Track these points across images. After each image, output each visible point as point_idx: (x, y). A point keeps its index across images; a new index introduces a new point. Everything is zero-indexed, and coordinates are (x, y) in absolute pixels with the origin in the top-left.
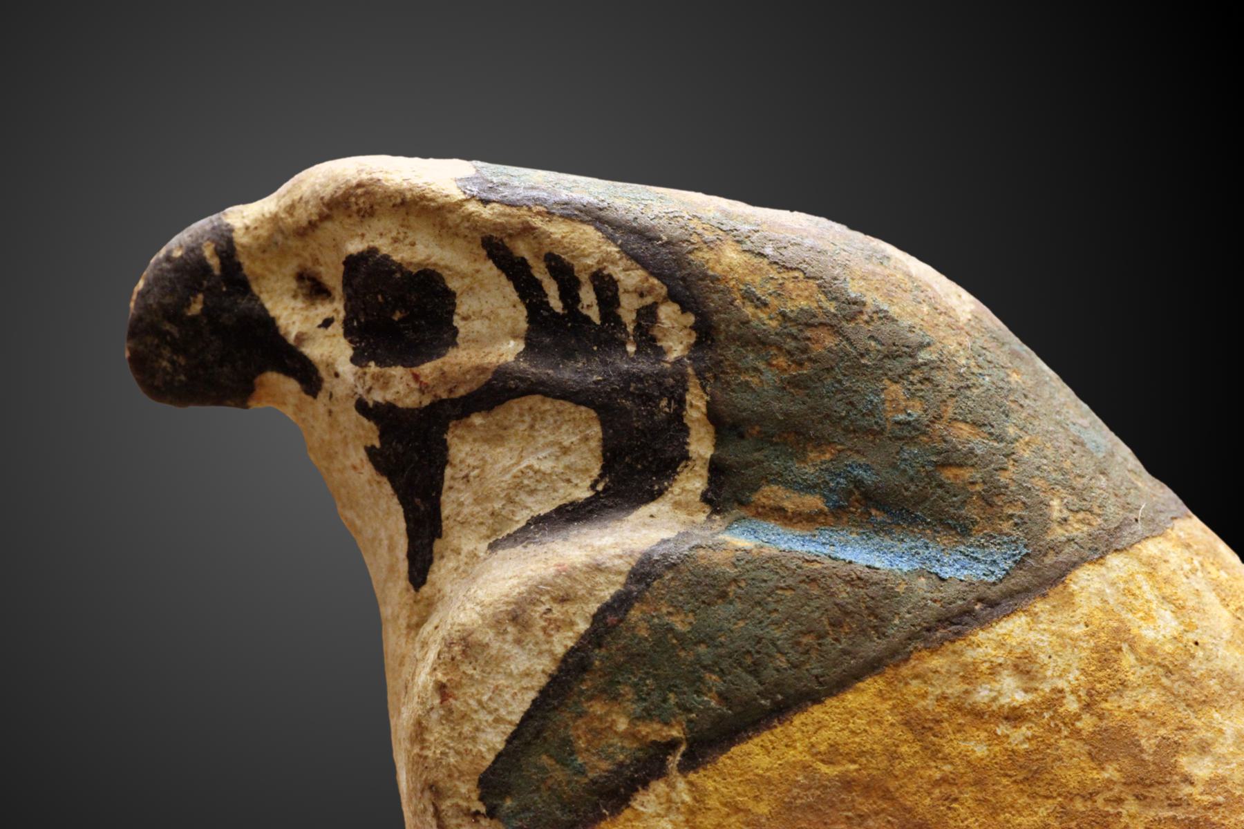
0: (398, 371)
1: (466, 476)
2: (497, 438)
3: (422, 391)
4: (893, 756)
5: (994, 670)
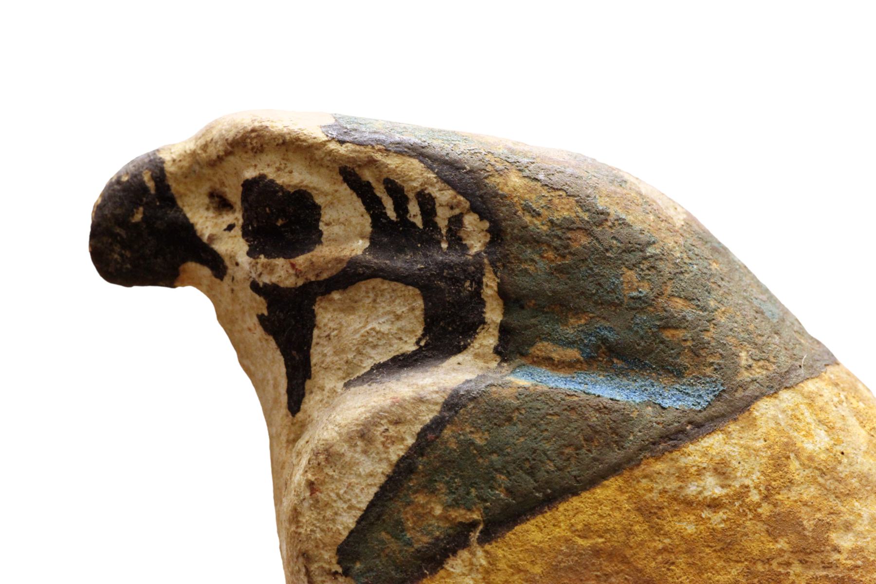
0: (280, 261)
1: (328, 336)
2: (350, 308)
3: (297, 276)
4: (629, 532)
5: (700, 472)
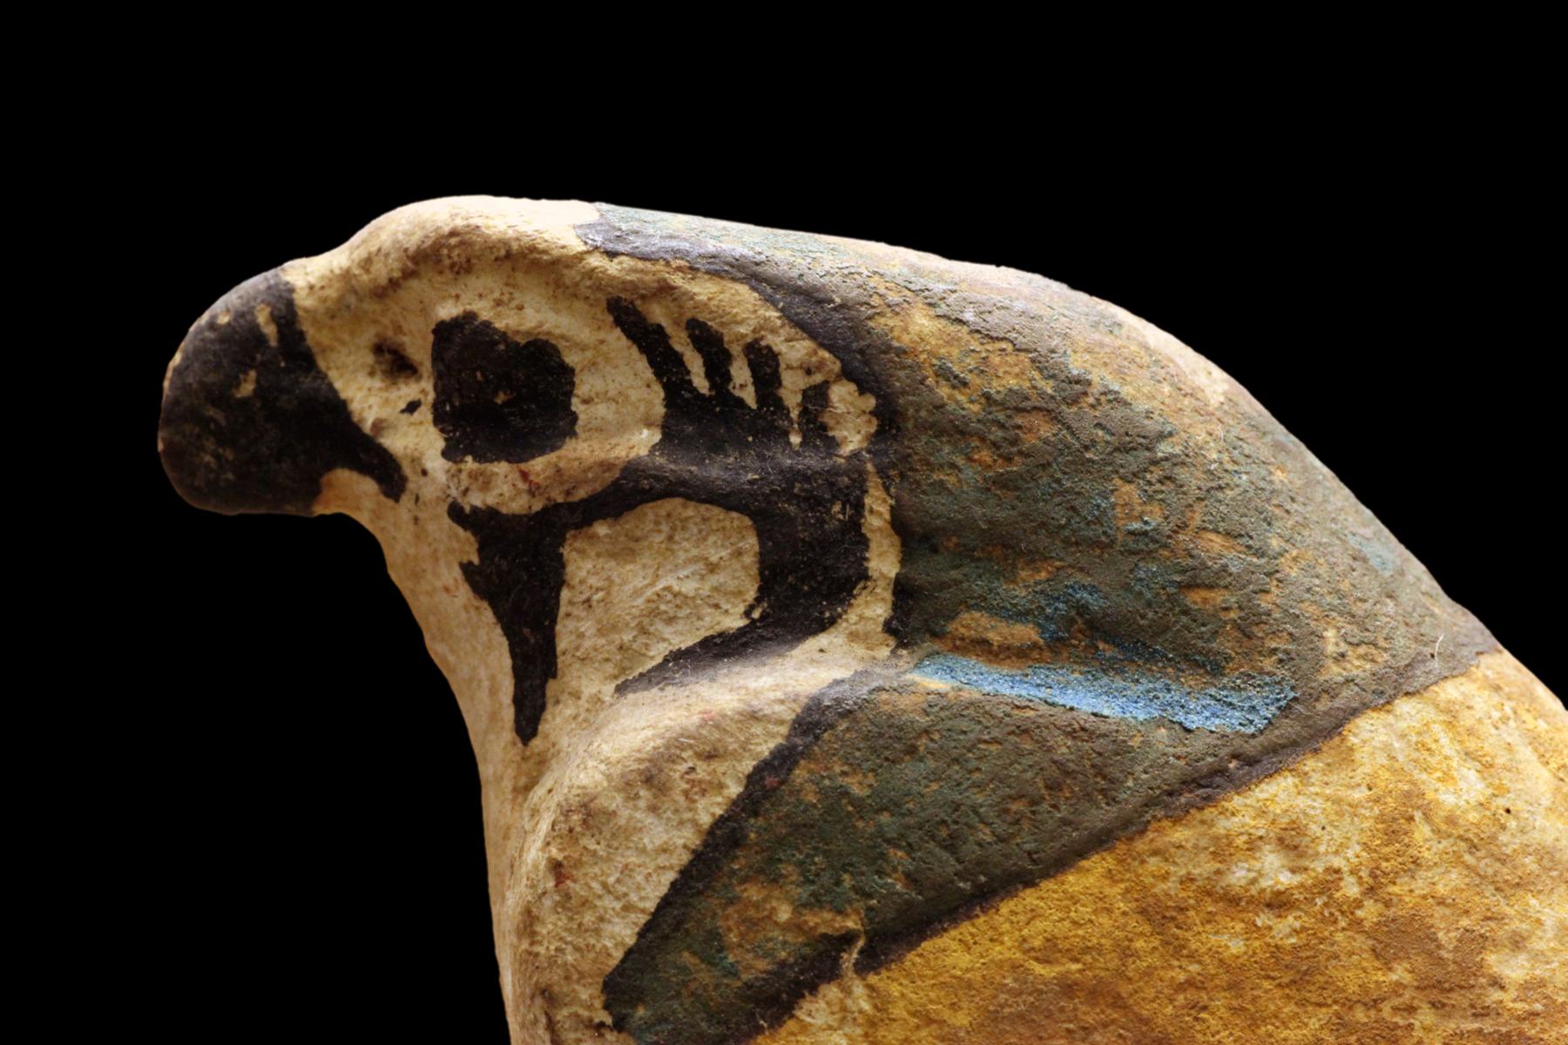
0: (501, 468)
1: (588, 600)
2: (626, 552)
3: (532, 493)
4: (1126, 952)
5: (1253, 845)
